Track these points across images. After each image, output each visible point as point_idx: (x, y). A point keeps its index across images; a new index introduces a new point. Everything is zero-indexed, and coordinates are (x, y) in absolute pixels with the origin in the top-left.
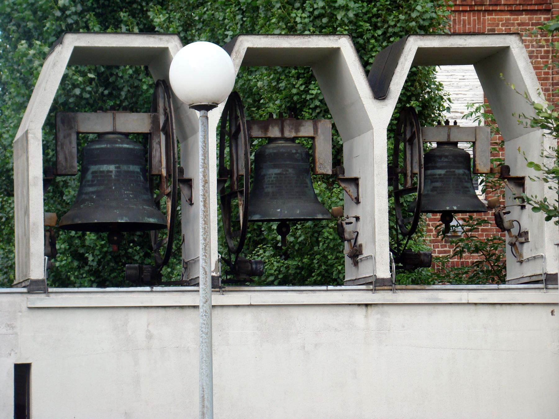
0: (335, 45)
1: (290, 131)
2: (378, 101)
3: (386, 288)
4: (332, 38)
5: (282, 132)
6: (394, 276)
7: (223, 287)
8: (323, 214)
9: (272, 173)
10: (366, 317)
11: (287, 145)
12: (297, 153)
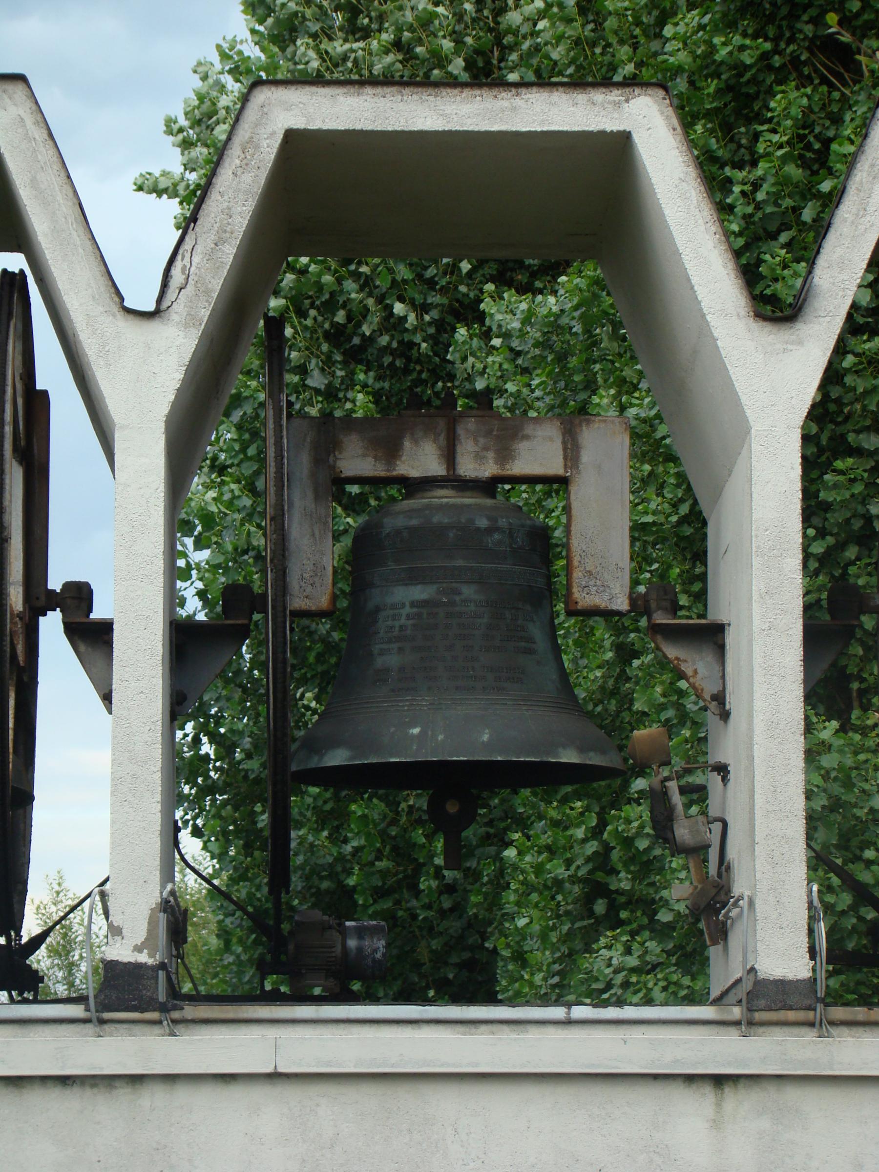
0: (611, 125)
1: (479, 457)
2: (768, 327)
3: (791, 1015)
4: (599, 96)
5: (450, 456)
6: (821, 975)
7: (175, 1008)
8: (582, 750)
9: (403, 597)
10: (716, 1124)
11: (459, 501)
12: (490, 531)
